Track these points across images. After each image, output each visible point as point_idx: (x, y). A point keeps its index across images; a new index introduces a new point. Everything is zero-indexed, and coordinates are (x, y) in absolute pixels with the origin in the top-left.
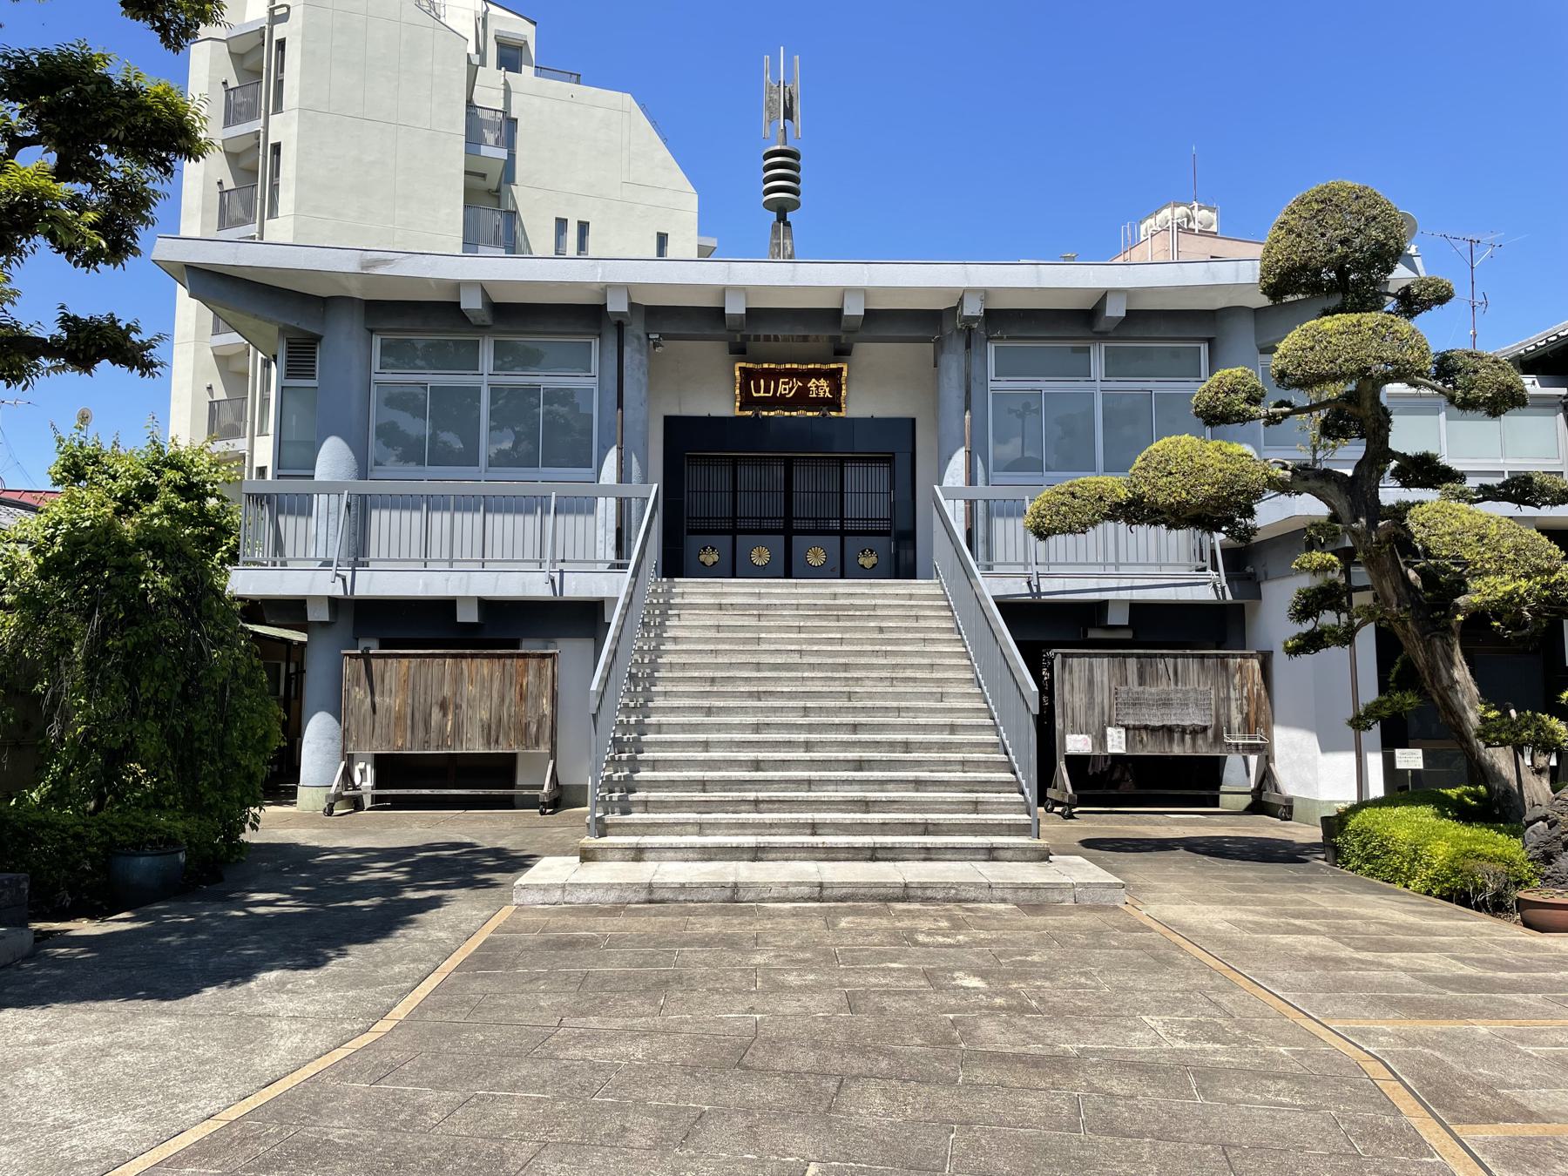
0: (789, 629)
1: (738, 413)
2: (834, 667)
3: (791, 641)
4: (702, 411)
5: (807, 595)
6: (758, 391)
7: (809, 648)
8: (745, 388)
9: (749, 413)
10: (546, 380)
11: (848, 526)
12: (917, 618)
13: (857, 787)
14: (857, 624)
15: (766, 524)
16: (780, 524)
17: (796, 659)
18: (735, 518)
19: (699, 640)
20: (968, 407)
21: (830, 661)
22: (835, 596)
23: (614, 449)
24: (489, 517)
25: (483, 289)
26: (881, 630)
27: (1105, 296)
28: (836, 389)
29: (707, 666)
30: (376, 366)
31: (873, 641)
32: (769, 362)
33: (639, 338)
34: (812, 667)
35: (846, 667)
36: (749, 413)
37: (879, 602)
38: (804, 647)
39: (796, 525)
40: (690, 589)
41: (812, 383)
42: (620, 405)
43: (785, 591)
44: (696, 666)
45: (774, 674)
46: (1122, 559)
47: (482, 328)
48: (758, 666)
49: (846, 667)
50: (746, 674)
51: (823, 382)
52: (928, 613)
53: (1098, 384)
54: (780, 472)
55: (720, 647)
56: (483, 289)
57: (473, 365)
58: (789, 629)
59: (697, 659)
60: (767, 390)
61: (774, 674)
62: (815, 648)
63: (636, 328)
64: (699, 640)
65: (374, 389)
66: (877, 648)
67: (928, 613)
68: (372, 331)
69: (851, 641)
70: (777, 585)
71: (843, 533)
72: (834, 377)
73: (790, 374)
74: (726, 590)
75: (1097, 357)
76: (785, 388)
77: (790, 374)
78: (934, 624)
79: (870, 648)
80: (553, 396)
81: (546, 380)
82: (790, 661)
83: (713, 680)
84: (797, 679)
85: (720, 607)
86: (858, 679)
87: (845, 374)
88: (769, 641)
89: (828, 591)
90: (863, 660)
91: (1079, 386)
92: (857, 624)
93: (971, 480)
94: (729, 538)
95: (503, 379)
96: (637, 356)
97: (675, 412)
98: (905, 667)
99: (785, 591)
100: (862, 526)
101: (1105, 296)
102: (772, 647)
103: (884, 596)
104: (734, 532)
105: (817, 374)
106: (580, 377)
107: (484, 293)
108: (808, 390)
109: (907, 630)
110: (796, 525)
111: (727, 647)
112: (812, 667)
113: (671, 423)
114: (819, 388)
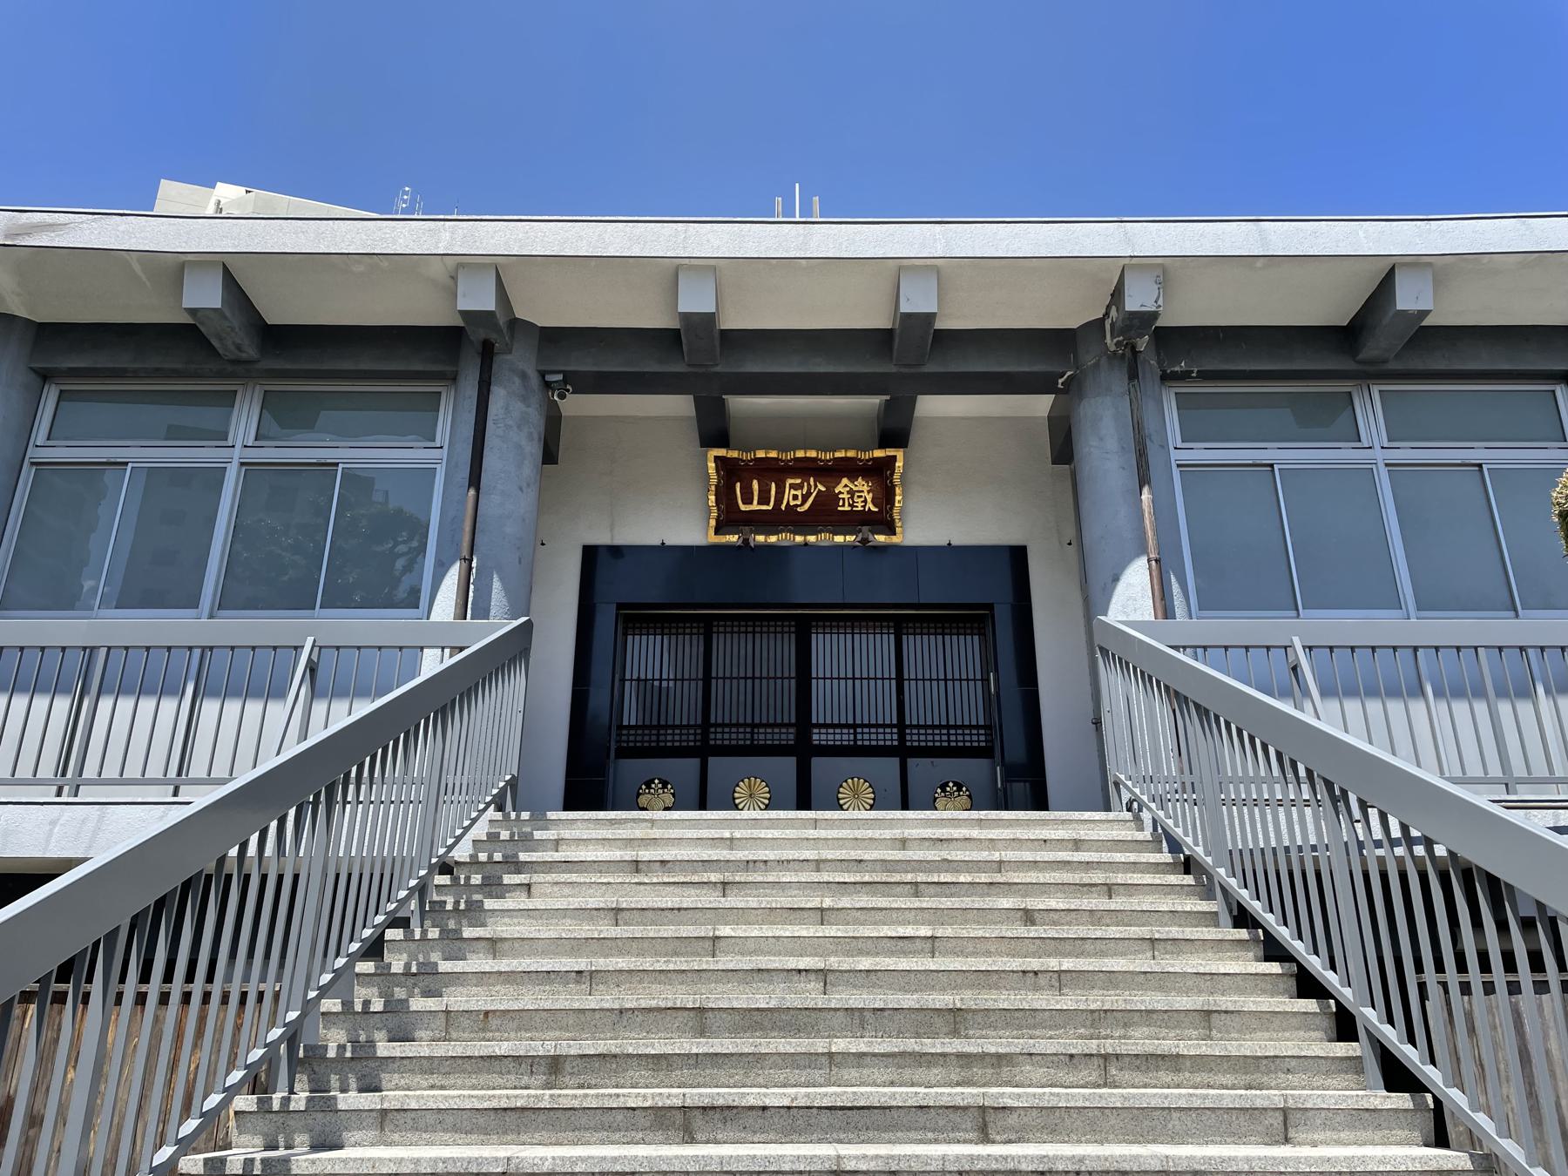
0: (795, 913)
1: (713, 539)
2: (924, 1021)
3: (799, 946)
4: (652, 539)
5: (840, 842)
6: (748, 501)
7: (846, 963)
8: (725, 495)
9: (733, 539)
10: (349, 455)
11: (913, 739)
12: (1109, 890)
13: (878, 1074)
14: (967, 902)
15: (763, 737)
16: (788, 737)
17: (811, 995)
18: (706, 725)
19: (557, 946)
20: (1144, 480)
21: (909, 1000)
22: (903, 843)
23: (456, 566)
24: (210, 708)
25: (227, 273)
26: (1028, 917)
27: (1390, 274)
28: (885, 495)
29: (551, 1019)
30: (40, 435)
31: (1013, 946)
32: (767, 448)
33: (524, 376)
34: (859, 1019)
35: (956, 1021)
36: (733, 539)
37: (1009, 855)
38: (834, 962)
39: (818, 737)
40: (589, 835)
41: (843, 487)
42: (475, 480)
43: (790, 833)
44: (521, 1020)
45: (744, 1045)
46: (1519, 770)
47: (240, 370)
48: (701, 1019)
49: (956, 1021)
50: (658, 1047)
51: (862, 485)
52: (1136, 878)
53: (1379, 454)
54: (787, 647)
55: (601, 963)
56: (227, 273)
57: (220, 435)
58: (795, 913)
59: (528, 999)
60: (764, 500)
61: (744, 1045)
62: (865, 963)
63: (519, 360)
64: (557, 946)
65: (28, 474)
66: (1034, 964)
67: (1136, 878)
68: (45, 376)
69: (959, 946)
70: (773, 824)
71: (903, 752)
72: (880, 472)
73: (806, 469)
74: (656, 833)
75: (1370, 413)
76: (796, 495)
77: (806, 469)
78: (1166, 904)
79: (1016, 964)
80: (358, 482)
81: (349, 455)
82: (793, 1001)
83: (555, 1067)
84: (811, 1060)
85: (636, 866)
86: (1000, 1059)
87: (899, 464)
88: (741, 945)
89: (888, 834)
90: (1005, 1000)
91: (1344, 454)
92: (967, 902)
93: (1165, 609)
94: (693, 764)
95: (269, 454)
96: (518, 407)
97: (601, 538)
98: (1128, 1019)
99: (790, 833)
100: (938, 739)
101: (1390, 274)
102: (746, 963)
103: (1016, 842)
104: (704, 751)
105: (850, 469)
106: (412, 455)
107: (231, 283)
108: (836, 498)
109: (1095, 917)
110: (818, 737)
111: (622, 963)
112: (859, 1019)
113: (590, 555)
114: (856, 494)
